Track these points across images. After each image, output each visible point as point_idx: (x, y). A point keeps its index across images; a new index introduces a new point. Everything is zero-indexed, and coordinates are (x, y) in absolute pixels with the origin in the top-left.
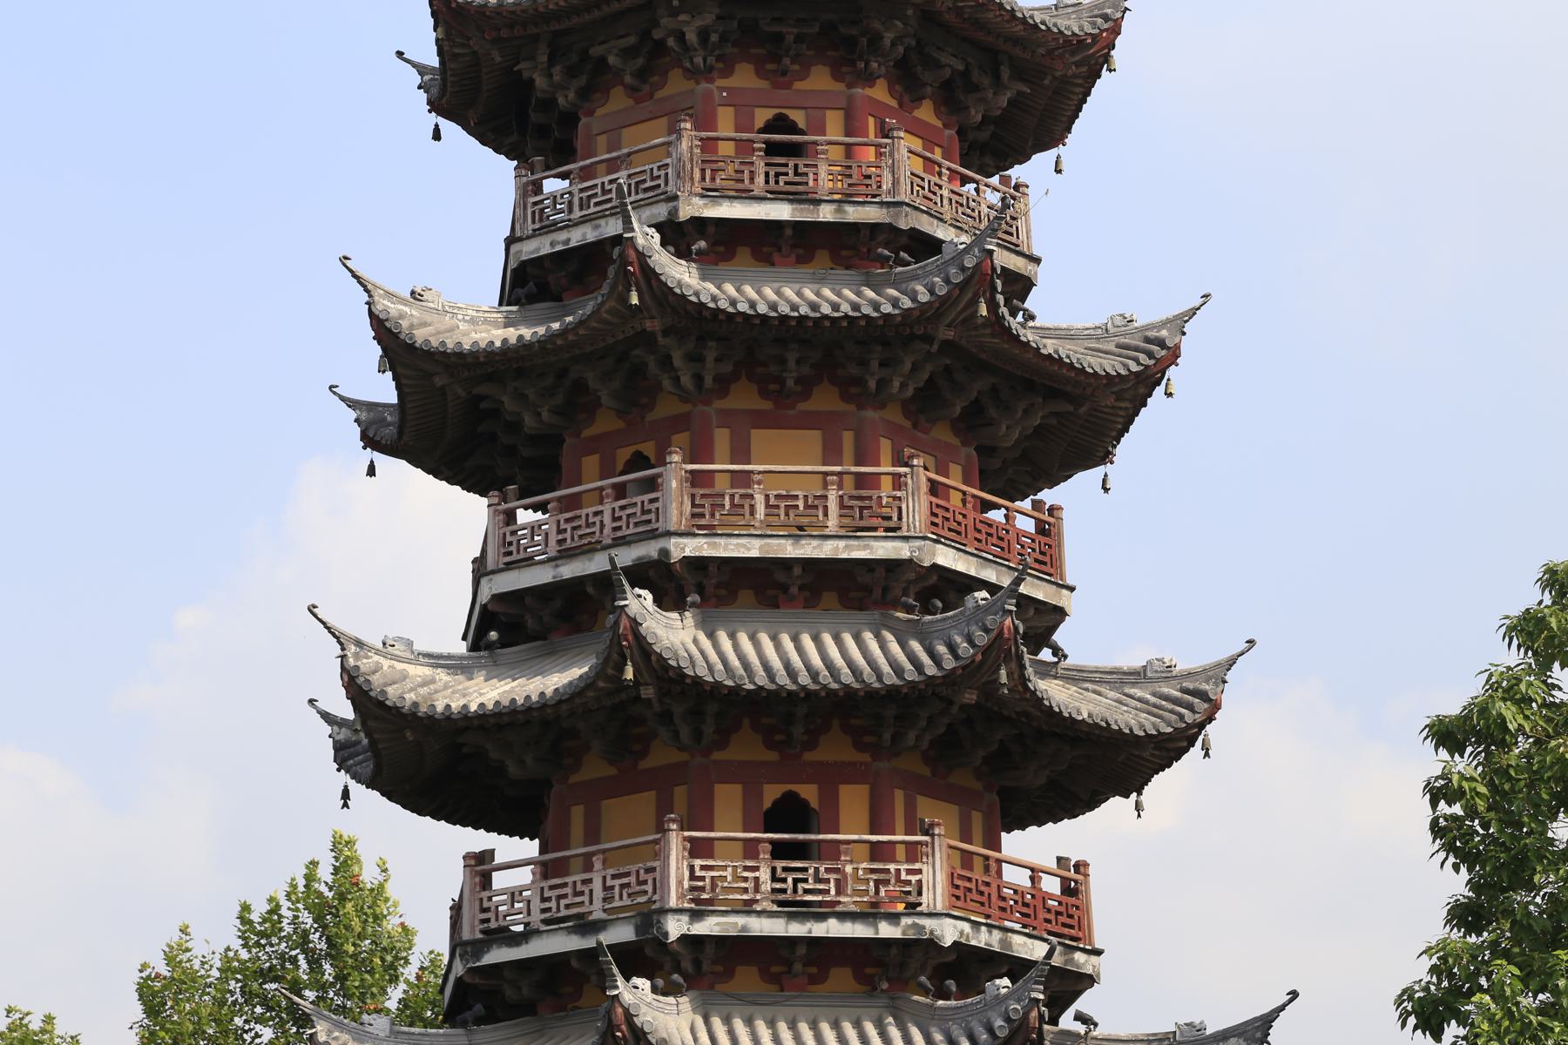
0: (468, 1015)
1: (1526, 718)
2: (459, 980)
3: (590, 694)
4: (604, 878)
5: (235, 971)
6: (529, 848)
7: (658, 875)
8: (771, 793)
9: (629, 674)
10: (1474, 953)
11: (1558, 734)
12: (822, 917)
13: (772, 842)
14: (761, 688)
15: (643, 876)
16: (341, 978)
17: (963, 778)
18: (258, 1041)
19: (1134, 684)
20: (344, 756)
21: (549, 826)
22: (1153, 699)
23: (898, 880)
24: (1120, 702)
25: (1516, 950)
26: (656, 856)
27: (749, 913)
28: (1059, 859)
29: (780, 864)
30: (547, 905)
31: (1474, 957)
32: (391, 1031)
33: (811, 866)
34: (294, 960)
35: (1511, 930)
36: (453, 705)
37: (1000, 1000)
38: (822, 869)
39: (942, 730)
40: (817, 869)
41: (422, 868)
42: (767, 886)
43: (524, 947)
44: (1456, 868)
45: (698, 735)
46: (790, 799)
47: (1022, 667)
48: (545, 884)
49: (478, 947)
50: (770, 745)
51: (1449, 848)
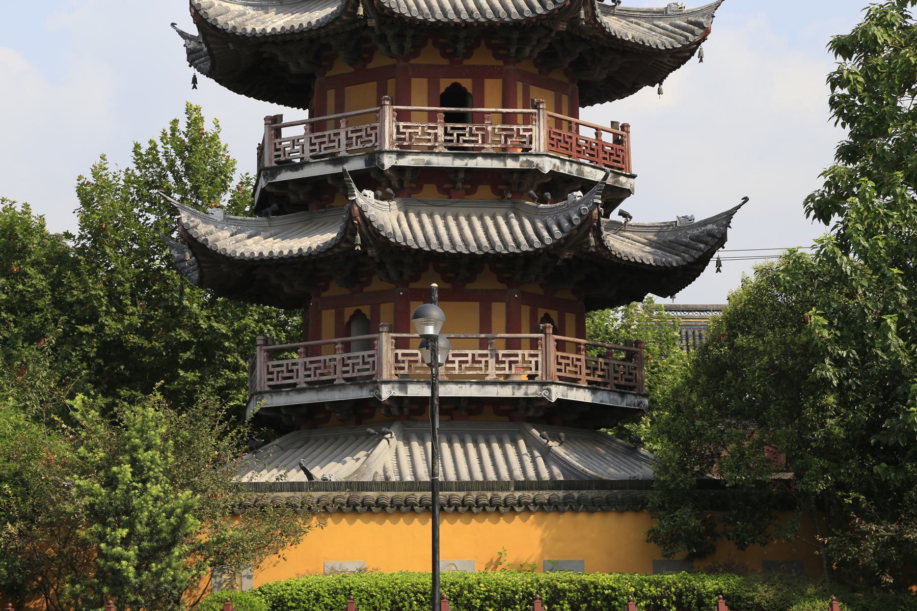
0: (268, 210)
1: (890, 36)
2: (263, 190)
3: (338, 23)
4: (347, 132)
5: (133, 183)
6: (303, 114)
7: (378, 131)
8: (445, 84)
9: (361, 11)
10: (851, 175)
11: (907, 45)
12: (473, 156)
13: (445, 112)
14: (439, 21)
15: (369, 132)
16: (195, 188)
17: (558, 75)
18: (148, 222)
19: (659, 19)
20: (193, 57)
21: (314, 101)
22: (670, 28)
23: (518, 134)
24: (651, 30)
25: (875, 172)
26: (377, 120)
27: (431, 153)
28: (612, 123)
29: (449, 125)
30: (313, 147)
31: (851, 176)
32: (224, 218)
33: (468, 127)
34: (165, 176)
35: (873, 160)
36: (257, 29)
37: (576, 204)
38: (474, 128)
39: (546, 46)
40: (471, 129)
41: (240, 124)
42: (442, 138)
43: (300, 171)
44: (843, 125)
45: (401, 49)
46: (456, 86)
47: (594, 9)
48: (313, 135)
49: (274, 171)
50: (444, 55)
51: (840, 114)
